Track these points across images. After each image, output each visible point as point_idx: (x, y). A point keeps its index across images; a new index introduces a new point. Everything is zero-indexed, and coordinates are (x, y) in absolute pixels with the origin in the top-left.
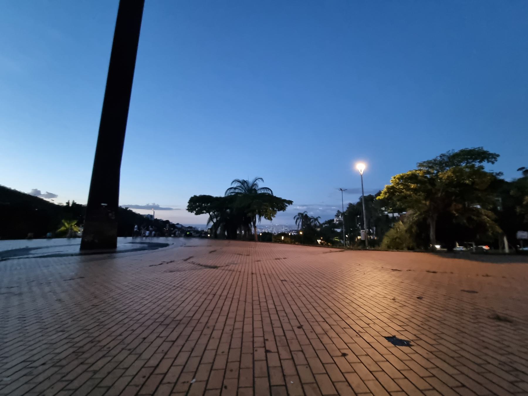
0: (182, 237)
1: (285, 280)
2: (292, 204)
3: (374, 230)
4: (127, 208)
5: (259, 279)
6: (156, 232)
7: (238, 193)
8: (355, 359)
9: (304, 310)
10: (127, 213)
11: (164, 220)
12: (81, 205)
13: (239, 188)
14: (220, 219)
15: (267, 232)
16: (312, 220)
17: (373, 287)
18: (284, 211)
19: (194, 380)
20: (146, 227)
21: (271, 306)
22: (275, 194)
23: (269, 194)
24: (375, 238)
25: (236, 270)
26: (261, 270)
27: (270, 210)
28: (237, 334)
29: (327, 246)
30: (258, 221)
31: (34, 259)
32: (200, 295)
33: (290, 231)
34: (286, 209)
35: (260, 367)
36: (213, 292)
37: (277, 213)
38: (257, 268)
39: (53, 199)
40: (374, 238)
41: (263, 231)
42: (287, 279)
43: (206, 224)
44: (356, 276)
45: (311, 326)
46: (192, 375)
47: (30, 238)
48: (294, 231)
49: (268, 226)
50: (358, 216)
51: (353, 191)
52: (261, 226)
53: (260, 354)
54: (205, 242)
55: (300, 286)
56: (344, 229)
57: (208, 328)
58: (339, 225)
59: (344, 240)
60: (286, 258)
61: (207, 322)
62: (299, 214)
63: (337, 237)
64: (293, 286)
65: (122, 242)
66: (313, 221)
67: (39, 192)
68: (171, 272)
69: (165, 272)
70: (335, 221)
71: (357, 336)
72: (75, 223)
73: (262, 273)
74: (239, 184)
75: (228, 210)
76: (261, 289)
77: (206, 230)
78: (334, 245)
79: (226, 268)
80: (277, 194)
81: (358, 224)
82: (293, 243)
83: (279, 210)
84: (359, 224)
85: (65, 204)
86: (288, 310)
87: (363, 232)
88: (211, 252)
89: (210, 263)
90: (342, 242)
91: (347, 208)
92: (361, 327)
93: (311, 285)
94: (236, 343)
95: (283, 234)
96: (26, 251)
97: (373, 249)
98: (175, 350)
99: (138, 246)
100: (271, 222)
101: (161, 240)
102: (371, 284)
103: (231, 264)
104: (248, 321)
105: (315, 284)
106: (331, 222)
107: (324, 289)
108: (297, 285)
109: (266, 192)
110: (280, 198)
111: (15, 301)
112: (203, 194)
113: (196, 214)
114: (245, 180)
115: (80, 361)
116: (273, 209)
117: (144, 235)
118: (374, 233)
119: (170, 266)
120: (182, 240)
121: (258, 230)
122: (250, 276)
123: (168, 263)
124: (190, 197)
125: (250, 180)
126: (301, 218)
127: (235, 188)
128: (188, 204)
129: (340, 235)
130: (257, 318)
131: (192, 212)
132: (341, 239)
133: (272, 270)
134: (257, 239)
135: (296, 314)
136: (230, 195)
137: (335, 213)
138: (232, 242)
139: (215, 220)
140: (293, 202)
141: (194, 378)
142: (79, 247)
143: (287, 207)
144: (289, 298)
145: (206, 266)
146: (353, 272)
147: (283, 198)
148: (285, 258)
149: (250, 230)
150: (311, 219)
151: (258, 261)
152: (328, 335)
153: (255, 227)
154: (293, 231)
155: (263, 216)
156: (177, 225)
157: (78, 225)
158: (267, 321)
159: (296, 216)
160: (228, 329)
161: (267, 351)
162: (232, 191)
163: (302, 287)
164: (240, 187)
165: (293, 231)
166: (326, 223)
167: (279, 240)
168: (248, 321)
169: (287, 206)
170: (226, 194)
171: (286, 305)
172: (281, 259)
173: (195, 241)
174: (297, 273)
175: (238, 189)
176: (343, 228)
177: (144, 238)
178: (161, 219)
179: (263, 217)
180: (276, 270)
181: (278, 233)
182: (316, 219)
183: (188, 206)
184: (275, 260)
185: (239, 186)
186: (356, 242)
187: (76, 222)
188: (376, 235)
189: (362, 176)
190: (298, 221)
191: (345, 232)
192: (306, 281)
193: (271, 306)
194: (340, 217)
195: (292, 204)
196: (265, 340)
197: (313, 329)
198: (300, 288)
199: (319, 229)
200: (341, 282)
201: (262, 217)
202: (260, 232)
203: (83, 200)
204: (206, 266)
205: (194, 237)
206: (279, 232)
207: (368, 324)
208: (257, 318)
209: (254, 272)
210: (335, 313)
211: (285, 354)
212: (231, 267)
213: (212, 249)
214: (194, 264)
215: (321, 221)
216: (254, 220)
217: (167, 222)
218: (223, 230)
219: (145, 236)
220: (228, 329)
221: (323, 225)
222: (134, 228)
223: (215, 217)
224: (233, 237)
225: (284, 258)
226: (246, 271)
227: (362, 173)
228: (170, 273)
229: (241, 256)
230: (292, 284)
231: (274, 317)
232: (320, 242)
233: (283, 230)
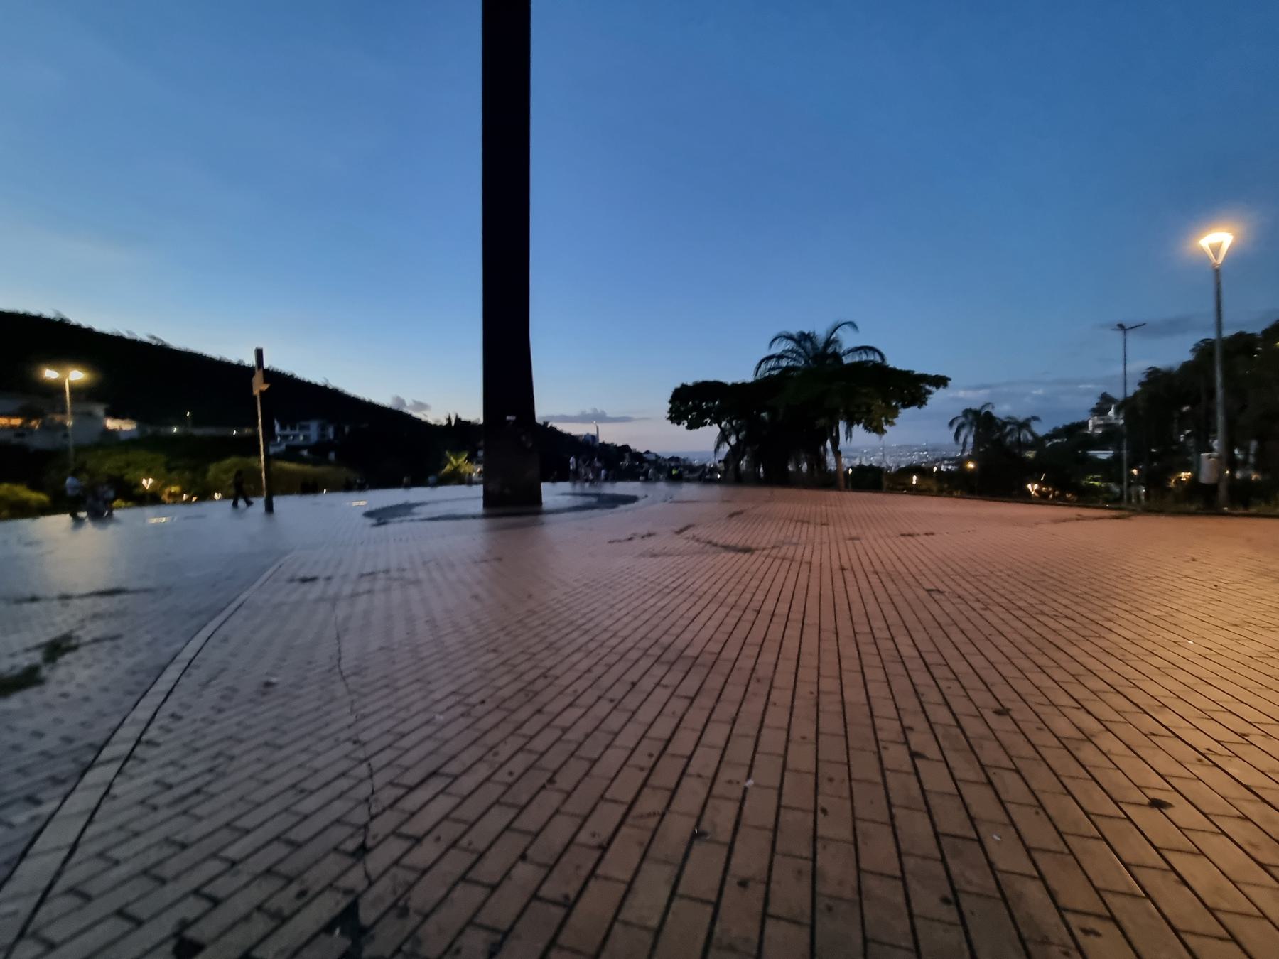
0: (661, 481)
1: (938, 591)
2: (945, 385)
3: (1252, 451)
4: (546, 423)
5: (863, 583)
6: (608, 470)
7: (788, 369)
8: (1197, 820)
9: (1009, 671)
10: (549, 435)
11: (620, 444)
12: (469, 422)
13: (789, 354)
14: (745, 437)
15: (865, 463)
16: (1009, 428)
17: (1254, 628)
18: (919, 407)
19: (750, 782)
20: (588, 462)
21: (908, 651)
22: (892, 362)
23: (875, 365)
24: (1254, 477)
25: (798, 557)
26: (866, 562)
27: (880, 406)
28: (830, 704)
29: (1060, 501)
30: (845, 439)
31: (420, 524)
32: (724, 610)
33: (937, 460)
34: (928, 402)
35: (903, 787)
36: (755, 604)
37: (899, 415)
38: (854, 557)
39: (426, 412)
40: (1249, 477)
41: (854, 462)
42: (942, 588)
43: (713, 450)
44: (1182, 592)
45: (1037, 715)
46: (745, 771)
47: (408, 486)
48: (946, 462)
49: (869, 450)
50: (1185, 409)
51: (1172, 327)
52: (855, 450)
53: (896, 756)
54: (715, 491)
55: (986, 609)
56: (1124, 452)
57: (758, 680)
58: (1109, 437)
59: (1125, 484)
60: (932, 534)
61: (753, 670)
62: (967, 412)
63: (1095, 476)
64: (963, 607)
65: (553, 494)
66: (1011, 430)
67: (402, 402)
68: (654, 556)
69: (642, 555)
70: (1090, 428)
71: (1200, 760)
72: (464, 459)
73: (869, 569)
74: (790, 345)
75: (764, 414)
76: (872, 606)
77: (710, 465)
78: (1086, 497)
79: (774, 552)
80: (896, 361)
81: (1181, 432)
82: (944, 493)
83: (905, 406)
84: (1188, 432)
85: (444, 422)
86: (960, 667)
87: (1212, 459)
88: (732, 515)
89: (735, 539)
90: (1116, 489)
91: (1141, 384)
92: (1217, 741)
93: (1020, 608)
94: (831, 723)
95: (912, 470)
96: (404, 510)
97: (1241, 511)
98: (696, 717)
99: (580, 501)
100: (880, 439)
101: (622, 488)
102: (1248, 620)
103: (784, 543)
104: (852, 678)
105: (1014, 602)
106: (1075, 430)
107: (1067, 622)
108: (977, 606)
109: (864, 357)
110: (908, 372)
111: (413, 592)
112: (701, 378)
113: (690, 427)
114: (807, 333)
115: (537, 706)
116: (889, 404)
117: (585, 477)
118: (1252, 459)
119: (650, 543)
120: (662, 487)
121: (844, 461)
122: (838, 576)
123: (643, 537)
124: (673, 390)
125: (821, 332)
126: (971, 424)
127: (780, 357)
128: (670, 406)
129: (1110, 470)
130: (875, 674)
131: (679, 424)
132: (1111, 481)
133: (898, 565)
134: (842, 483)
135: (988, 680)
136: (767, 374)
137: (1093, 402)
138: (779, 492)
139: (733, 440)
140: (950, 379)
141: (749, 776)
142: (481, 502)
143: (931, 396)
144: (957, 637)
145: (727, 548)
146: (1172, 580)
147: (917, 372)
148: (928, 532)
149: (821, 461)
150: (1005, 424)
151: (852, 539)
152: (622, 696)
153: (837, 454)
154: (944, 459)
155: (858, 423)
156: (645, 456)
157: (470, 459)
158: (901, 684)
159: (956, 418)
160: (805, 690)
161: (914, 755)
162: (772, 363)
163: (991, 610)
164: (792, 351)
165: (944, 459)
166: (1056, 433)
167: (904, 484)
168: (852, 678)
169: (930, 392)
170: (759, 374)
171: (950, 652)
172: (918, 535)
173: (689, 490)
174: (973, 573)
175: (788, 358)
176: (1119, 448)
177: (587, 485)
178: (612, 444)
179: (861, 425)
180: (908, 564)
181: (898, 466)
182: (1025, 425)
183: (671, 411)
184: (902, 539)
185: (788, 351)
186: (1170, 489)
187: (466, 455)
188: (1257, 468)
189: (1217, 272)
190: (963, 433)
191: (1128, 459)
192: (1002, 596)
193: (908, 651)
194: (1111, 413)
195: (945, 385)
196: (905, 729)
197: (1043, 722)
198: (987, 614)
199: (1030, 454)
200: (1126, 607)
201: (855, 426)
202: (849, 465)
203: (474, 412)
204: (727, 548)
205: (688, 480)
206: (903, 466)
207: (1242, 736)
208: (875, 674)
209: (846, 566)
210: (1116, 690)
211: (966, 770)
212: (788, 551)
213: (734, 508)
214: (698, 540)
215: (1041, 429)
216: (834, 435)
217: (626, 448)
218: (754, 463)
219: (587, 480)
220: (805, 690)
221: (1046, 441)
222: (569, 464)
223: (732, 431)
224: (778, 478)
225: (927, 534)
226: (826, 563)
227: (1220, 261)
228: (651, 559)
229: (805, 525)
230: (959, 600)
231: (921, 678)
232: (1036, 491)
233: (915, 459)
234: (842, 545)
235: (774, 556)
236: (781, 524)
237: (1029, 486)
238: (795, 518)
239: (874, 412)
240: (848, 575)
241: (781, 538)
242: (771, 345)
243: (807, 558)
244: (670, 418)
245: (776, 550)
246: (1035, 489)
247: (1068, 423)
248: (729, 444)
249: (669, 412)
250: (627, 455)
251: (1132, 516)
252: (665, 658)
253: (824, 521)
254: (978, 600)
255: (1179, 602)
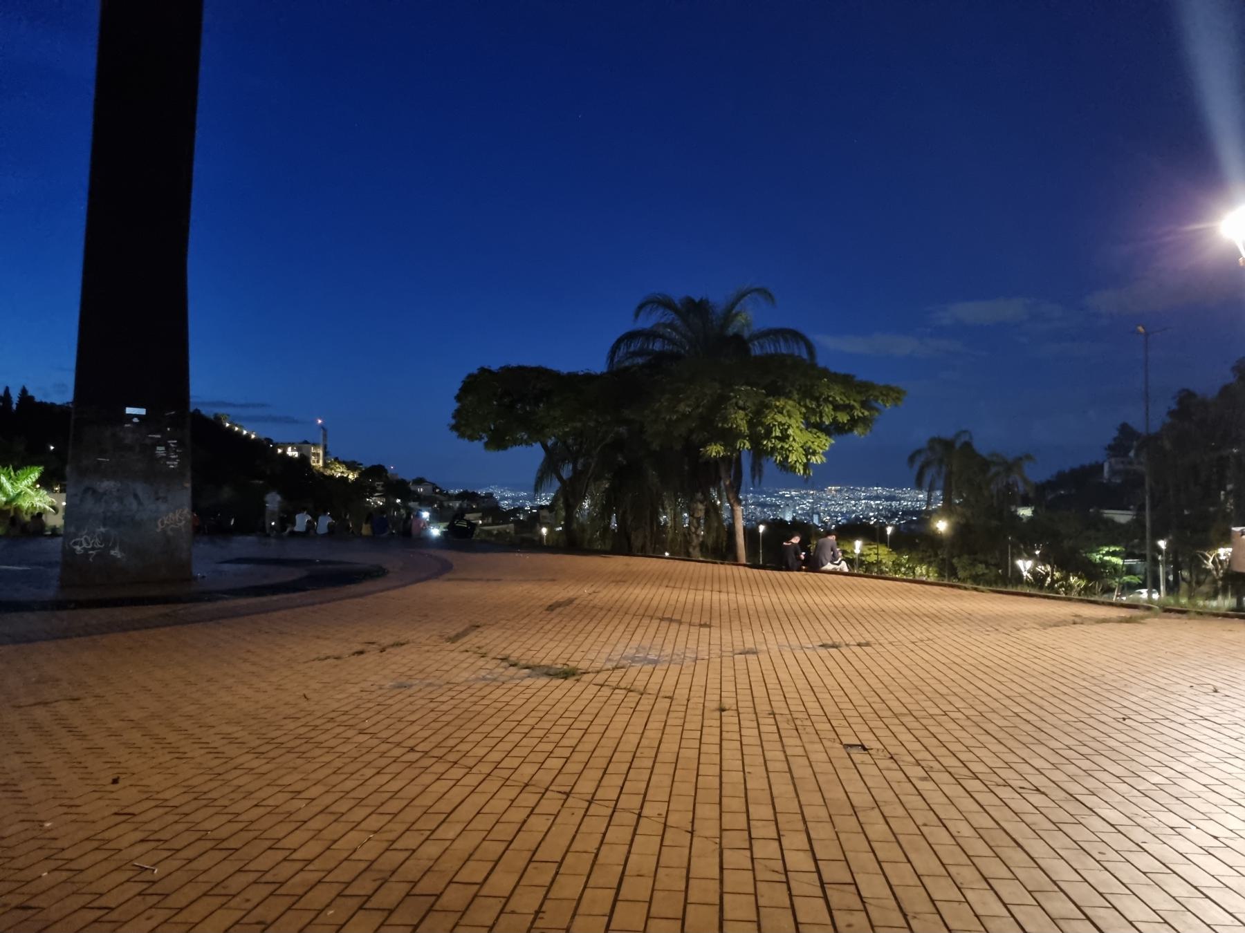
16: (993, 470)
25: (653, 688)
26: (759, 691)
36: (564, 781)
63: (1112, 549)
73: (763, 707)
79: (615, 678)
109: (783, 349)
124: (463, 376)
125: (718, 298)
127: (650, 335)
137: (1110, 434)
176: (1141, 508)
182: (1010, 467)
183: (458, 414)
185: (666, 325)
186: (1208, 572)
209: (729, 702)
229: (674, 626)
234: (727, 661)
235: (614, 684)
236: (635, 623)
237: (1020, 563)
238: (659, 614)
239: (791, 439)
240: (729, 718)
241: (630, 652)
242: (637, 315)
243: (668, 689)
244: (455, 428)
245: (619, 673)
246: (1028, 568)
247: (1076, 465)
248: (560, 478)
249: (454, 417)
250: (379, 485)
251: (1147, 617)
252: (380, 900)
253: (705, 620)
254: (918, 763)
255: (1190, 761)
